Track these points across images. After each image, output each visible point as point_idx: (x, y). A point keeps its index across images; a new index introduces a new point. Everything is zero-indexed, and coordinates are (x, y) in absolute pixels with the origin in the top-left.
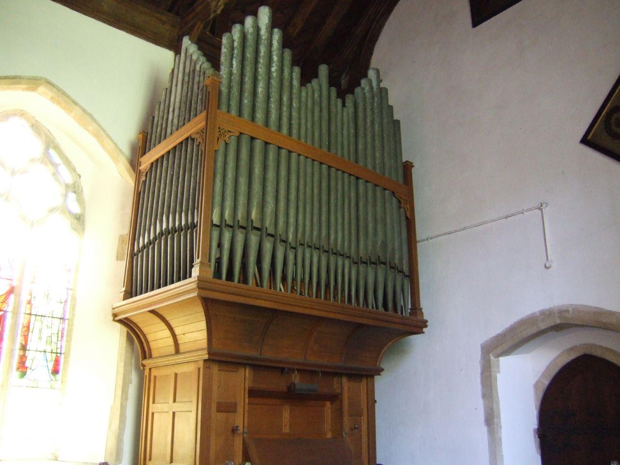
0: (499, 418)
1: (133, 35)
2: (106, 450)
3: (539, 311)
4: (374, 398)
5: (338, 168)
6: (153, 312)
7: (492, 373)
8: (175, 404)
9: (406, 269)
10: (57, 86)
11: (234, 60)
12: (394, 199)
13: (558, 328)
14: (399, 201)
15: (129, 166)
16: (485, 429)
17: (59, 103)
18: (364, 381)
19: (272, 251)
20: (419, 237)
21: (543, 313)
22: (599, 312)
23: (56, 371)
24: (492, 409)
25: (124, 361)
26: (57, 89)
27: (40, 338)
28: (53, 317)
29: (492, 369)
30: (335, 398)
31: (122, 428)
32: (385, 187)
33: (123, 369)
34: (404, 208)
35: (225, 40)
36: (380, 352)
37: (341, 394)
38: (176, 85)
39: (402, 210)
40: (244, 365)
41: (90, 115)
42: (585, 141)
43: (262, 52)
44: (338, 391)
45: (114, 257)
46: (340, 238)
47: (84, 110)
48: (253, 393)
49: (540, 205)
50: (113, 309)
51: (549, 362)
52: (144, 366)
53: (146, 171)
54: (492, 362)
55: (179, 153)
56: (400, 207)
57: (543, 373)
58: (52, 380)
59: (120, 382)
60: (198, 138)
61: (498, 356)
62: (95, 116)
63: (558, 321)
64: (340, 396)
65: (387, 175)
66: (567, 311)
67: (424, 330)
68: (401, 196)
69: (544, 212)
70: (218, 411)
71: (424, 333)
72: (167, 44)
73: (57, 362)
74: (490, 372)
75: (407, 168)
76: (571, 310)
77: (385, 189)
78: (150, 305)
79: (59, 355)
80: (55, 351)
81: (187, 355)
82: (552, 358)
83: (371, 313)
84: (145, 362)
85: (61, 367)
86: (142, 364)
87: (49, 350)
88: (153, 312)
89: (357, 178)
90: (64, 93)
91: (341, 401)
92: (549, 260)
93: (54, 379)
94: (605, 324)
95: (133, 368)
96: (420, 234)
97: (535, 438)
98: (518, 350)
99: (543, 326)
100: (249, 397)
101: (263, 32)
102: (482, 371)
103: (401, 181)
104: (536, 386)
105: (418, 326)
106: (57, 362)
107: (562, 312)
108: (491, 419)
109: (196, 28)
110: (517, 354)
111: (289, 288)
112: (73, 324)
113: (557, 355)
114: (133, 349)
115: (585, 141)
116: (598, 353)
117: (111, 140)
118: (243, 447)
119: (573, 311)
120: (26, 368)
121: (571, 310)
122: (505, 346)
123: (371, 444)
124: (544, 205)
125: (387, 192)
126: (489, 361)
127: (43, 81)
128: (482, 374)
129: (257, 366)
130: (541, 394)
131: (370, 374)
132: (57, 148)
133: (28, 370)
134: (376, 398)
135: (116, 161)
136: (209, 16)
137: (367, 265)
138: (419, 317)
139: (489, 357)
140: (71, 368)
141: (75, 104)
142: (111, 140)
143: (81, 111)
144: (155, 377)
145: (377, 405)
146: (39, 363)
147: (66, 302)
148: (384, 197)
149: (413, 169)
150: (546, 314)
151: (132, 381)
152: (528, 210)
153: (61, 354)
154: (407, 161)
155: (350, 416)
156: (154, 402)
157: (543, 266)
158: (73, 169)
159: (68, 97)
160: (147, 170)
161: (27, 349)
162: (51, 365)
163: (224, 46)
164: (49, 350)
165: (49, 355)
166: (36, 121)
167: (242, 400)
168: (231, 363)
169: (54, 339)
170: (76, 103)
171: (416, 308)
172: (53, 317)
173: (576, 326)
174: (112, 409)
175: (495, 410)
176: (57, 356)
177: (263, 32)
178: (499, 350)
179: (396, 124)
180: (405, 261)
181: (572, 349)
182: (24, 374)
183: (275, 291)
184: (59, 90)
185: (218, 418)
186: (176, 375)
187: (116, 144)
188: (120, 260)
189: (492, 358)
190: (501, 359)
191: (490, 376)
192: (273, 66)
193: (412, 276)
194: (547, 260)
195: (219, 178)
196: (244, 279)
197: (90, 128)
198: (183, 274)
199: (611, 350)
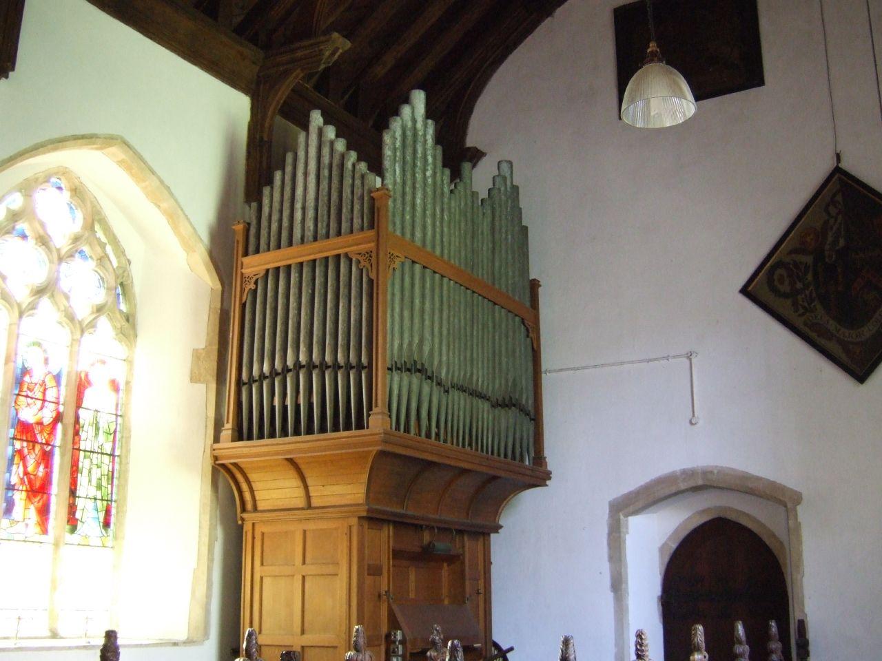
0: (627, 584)
1: (195, 64)
2: (189, 623)
3: (680, 470)
4: (490, 559)
5: (468, 286)
6: (291, 461)
7: (622, 535)
8: (304, 566)
9: (531, 408)
10: (134, 148)
11: (397, 165)
12: (523, 326)
13: (696, 489)
14: (527, 330)
15: (208, 259)
16: (611, 595)
17: (128, 169)
18: (481, 539)
19: (418, 395)
20: (543, 368)
21: (684, 472)
22: (746, 477)
23: (107, 524)
24: (620, 574)
25: (209, 513)
26: (134, 152)
27: (90, 481)
28: (102, 453)
29: (622, 530)
30: (453, 559)
31: (209, 596)
32: (436, 270)
33: (208, 523)
34: (531, 338)
35: (387, 138)
36: (500, 505)
37: (463, 555)
38: (306, 174)
39: (529, 340)
40: (388, 522)
41: (168, 188)
42: (745, 291)
43: (420, 152)
44: (460, 551)
45: (187, 378)
46: (480, 379)
47: (162, 182)
48: (397, 554)
49: (689, 354)
50: (214, 450)
51: (677, 525)
52: (243, 519)
53: (255, 278)
54: (621, 522)
55: (323, 268)
56: (528, 336)
57: (670, 536)
58: (103, 535)
59: (206, 540)
60: (362, 261)
61: (627, 515)
62: (173, 190)
63: (700, 482)
64: (461, 557)
65: (497, 286)
66: (711, 472)
67: (548, 482)
68: (530, 323)
69: (693, 361)
70: (368, 575)
71: (547, 485)
72: (244, 86)
73: (108, 512)
74: (620, 532)
75: (534, 286)
76: (716, 472)
77: (435, 272)
78: (290, 452)
79: (109, 503)
80: (105, 498)
81: (317, 511)
82: (681, 521)
83: (390, 435)
84: (245, 515)
85: (113, 519)
86: (241, 517)
87: (99, 497)
88: (291, 461)
89: (443, 276)
90: (141, 158)
91: (463, 563)
92: (696, 415)
93: (106, 535)
94: (751, 488)
95: (218, 522)
96: (545, 365)
97: (658, 605)
98: (647, 511)
99: (683, 486)
100: (393, 558)
101: (419, 125)
102: (609, 531)
103: (528, 304)
104: (662, 550)
105: (538, 476)
106: (108, 512)
107: (706, 473)
108: (618, 585)
109: (294, 75)
110: (648, 513)
111: (474, 448)
112: (128, 463)
113: (687, 516)
114: (217, 498)
115: (745, 291)
116: (732, 517)
117: (191, 224)
118: (388, 614)
119: (718, 473)
120: (77, 520)
121: (716, 472)
122: (640, 504)
123: (487, 609)
124: (694, 355)
125: (452, 282)
126: (618, 521)
127: (119, 141)
128: (610, 534)
129: (401, 524)
130: (667, 559)
131: (485, 531)
132: (104, 222)
133: (79, 523)
134: (492, 560)
135: (188, 247)
136: (318, 66)
137: (392, 372)
138: (543, 468)
139: (619, 516)
140: (131, 518)
141: (153, 173)
142: (191, 224)
143: (158, 183)
144: (263, 534)
145: (492, 566)
146: (88, 512)
147: (115, 432)
148: (433, 280)
149: (540, 288)
150: (689, 474)
151: (217, 538)
152: (674, 357)
153: (111, 501)
154: (534, 280)
155: (470, 579)
156: (262, 564)
157: (688, 421)
158: (120, 252)
159: (145, 163)
160: (257, 277)
161: (77, 495)
162: (102, 516)
163: (387, 147)
164: (99, 497)
165: (99, 502)
166: (81, 183)
167: (386, 561)
168: (377, 519)
169: (104, 483)
170: (153, 172)
171: (539, 459)
172: (102, 453)
173: (714, 487)
174: (194, 573)
175: (623, 574)
176: (108, 504)
177: (419, 125)
178: (631, 509)
179: (524, 230)
180: (531, 402)
181: (704, 511)
182: (73, 529)
183: (438, 442)
184: (135, 152)
185: (369, 580)
186: (305, 532)
187: (194, 228)
188: (196, 383)
189: (622, 517)
190: (630, 518)
191: (620, 537)
192: (428, 170)
193: (535, 417)
194: (694, 416)
195: (389, 311)
196: (407, 430)
197: (164, 205)
198: (343, 418)
199: (748, 515)
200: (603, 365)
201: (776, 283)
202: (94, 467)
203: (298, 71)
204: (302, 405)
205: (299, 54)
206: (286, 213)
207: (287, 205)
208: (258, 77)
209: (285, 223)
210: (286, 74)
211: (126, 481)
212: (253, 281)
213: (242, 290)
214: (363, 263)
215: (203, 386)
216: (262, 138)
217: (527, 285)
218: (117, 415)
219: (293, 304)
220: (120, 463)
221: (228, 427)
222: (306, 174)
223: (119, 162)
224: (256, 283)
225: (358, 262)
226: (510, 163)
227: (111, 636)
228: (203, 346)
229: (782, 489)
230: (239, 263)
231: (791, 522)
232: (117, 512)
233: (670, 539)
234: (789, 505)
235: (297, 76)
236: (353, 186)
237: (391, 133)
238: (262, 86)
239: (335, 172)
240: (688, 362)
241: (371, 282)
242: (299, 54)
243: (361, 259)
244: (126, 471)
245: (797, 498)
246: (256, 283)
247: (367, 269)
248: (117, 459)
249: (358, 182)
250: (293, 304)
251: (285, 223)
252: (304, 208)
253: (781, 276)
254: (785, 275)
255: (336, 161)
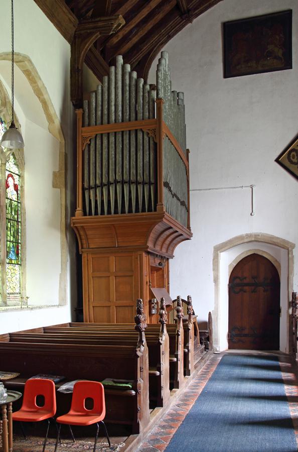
21: (247, 235)
42: (277, 161)
45: (51, 185)
61: (220, 252)
66: (259, 235)
67: (191, 238)
99: (246, 240)
107: (256, 235)
108: (216, 280)
112: (25, 225)
116: (260, 253)
126: (218, 254)
150: (248, 236)
200: (213, 189)
201: (291, 158)
202: (12, 227)
203: (98, 33)
204: (92, 200)
205: (100, 24)
206: (106, 107)
207: (106, 103)
208: (75, 34)
209: (106, 112)
210: (91, 34)
211: (25, 234)
212: (89, 139)
213: (83, 144)
214: (150, 135)
215: (59, 190)
216: (78, 68)
217: (186, 151)
218: (18, 203)
219: (112, 152)
220: (21, 225)
221: (79, 208)
222: (116, 88)
223: (24, 71)
224: (90, 140)
225: (148, 134)
226: (183, 93)
227: (210, 313)
228: (58, 171)
229: (288, 242)
230: (80, 131)
231: (290, 255)
232: (22, 248)
233: (233, 262)
234: (290, 249)
235: (97, 36)
236: (143, 96)
237: (160, 72)
238: (77, 40)
239: (133, 88)
240: (251, 189)
241: (155, 144)
242: (100, 24)
243: (149, 131)
244: (25, 229)
245: (293, 246)
246: (90, 140)
247: (153, 138)
248: (19, 224)
249: (147, 95)
250: (112, 152)
251: (106, 112)
252: (116, 105)
253: (294, 155)
254: (295, 155)
255: (133, 82)
